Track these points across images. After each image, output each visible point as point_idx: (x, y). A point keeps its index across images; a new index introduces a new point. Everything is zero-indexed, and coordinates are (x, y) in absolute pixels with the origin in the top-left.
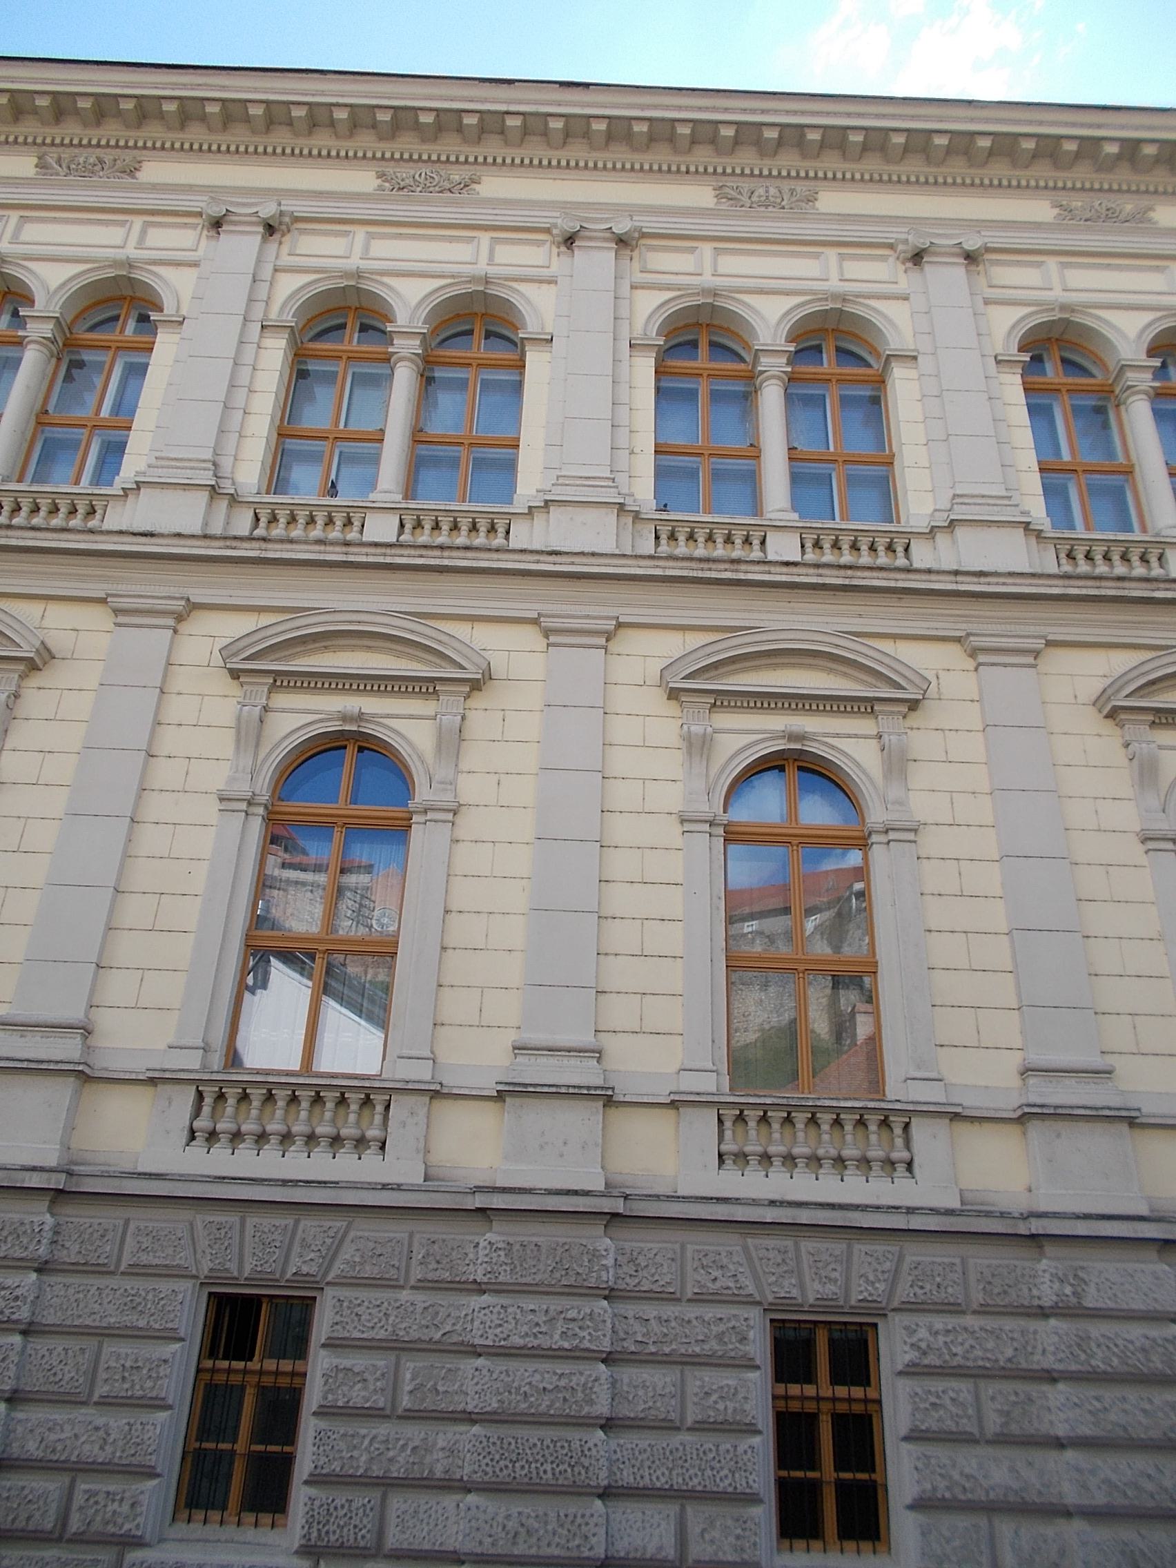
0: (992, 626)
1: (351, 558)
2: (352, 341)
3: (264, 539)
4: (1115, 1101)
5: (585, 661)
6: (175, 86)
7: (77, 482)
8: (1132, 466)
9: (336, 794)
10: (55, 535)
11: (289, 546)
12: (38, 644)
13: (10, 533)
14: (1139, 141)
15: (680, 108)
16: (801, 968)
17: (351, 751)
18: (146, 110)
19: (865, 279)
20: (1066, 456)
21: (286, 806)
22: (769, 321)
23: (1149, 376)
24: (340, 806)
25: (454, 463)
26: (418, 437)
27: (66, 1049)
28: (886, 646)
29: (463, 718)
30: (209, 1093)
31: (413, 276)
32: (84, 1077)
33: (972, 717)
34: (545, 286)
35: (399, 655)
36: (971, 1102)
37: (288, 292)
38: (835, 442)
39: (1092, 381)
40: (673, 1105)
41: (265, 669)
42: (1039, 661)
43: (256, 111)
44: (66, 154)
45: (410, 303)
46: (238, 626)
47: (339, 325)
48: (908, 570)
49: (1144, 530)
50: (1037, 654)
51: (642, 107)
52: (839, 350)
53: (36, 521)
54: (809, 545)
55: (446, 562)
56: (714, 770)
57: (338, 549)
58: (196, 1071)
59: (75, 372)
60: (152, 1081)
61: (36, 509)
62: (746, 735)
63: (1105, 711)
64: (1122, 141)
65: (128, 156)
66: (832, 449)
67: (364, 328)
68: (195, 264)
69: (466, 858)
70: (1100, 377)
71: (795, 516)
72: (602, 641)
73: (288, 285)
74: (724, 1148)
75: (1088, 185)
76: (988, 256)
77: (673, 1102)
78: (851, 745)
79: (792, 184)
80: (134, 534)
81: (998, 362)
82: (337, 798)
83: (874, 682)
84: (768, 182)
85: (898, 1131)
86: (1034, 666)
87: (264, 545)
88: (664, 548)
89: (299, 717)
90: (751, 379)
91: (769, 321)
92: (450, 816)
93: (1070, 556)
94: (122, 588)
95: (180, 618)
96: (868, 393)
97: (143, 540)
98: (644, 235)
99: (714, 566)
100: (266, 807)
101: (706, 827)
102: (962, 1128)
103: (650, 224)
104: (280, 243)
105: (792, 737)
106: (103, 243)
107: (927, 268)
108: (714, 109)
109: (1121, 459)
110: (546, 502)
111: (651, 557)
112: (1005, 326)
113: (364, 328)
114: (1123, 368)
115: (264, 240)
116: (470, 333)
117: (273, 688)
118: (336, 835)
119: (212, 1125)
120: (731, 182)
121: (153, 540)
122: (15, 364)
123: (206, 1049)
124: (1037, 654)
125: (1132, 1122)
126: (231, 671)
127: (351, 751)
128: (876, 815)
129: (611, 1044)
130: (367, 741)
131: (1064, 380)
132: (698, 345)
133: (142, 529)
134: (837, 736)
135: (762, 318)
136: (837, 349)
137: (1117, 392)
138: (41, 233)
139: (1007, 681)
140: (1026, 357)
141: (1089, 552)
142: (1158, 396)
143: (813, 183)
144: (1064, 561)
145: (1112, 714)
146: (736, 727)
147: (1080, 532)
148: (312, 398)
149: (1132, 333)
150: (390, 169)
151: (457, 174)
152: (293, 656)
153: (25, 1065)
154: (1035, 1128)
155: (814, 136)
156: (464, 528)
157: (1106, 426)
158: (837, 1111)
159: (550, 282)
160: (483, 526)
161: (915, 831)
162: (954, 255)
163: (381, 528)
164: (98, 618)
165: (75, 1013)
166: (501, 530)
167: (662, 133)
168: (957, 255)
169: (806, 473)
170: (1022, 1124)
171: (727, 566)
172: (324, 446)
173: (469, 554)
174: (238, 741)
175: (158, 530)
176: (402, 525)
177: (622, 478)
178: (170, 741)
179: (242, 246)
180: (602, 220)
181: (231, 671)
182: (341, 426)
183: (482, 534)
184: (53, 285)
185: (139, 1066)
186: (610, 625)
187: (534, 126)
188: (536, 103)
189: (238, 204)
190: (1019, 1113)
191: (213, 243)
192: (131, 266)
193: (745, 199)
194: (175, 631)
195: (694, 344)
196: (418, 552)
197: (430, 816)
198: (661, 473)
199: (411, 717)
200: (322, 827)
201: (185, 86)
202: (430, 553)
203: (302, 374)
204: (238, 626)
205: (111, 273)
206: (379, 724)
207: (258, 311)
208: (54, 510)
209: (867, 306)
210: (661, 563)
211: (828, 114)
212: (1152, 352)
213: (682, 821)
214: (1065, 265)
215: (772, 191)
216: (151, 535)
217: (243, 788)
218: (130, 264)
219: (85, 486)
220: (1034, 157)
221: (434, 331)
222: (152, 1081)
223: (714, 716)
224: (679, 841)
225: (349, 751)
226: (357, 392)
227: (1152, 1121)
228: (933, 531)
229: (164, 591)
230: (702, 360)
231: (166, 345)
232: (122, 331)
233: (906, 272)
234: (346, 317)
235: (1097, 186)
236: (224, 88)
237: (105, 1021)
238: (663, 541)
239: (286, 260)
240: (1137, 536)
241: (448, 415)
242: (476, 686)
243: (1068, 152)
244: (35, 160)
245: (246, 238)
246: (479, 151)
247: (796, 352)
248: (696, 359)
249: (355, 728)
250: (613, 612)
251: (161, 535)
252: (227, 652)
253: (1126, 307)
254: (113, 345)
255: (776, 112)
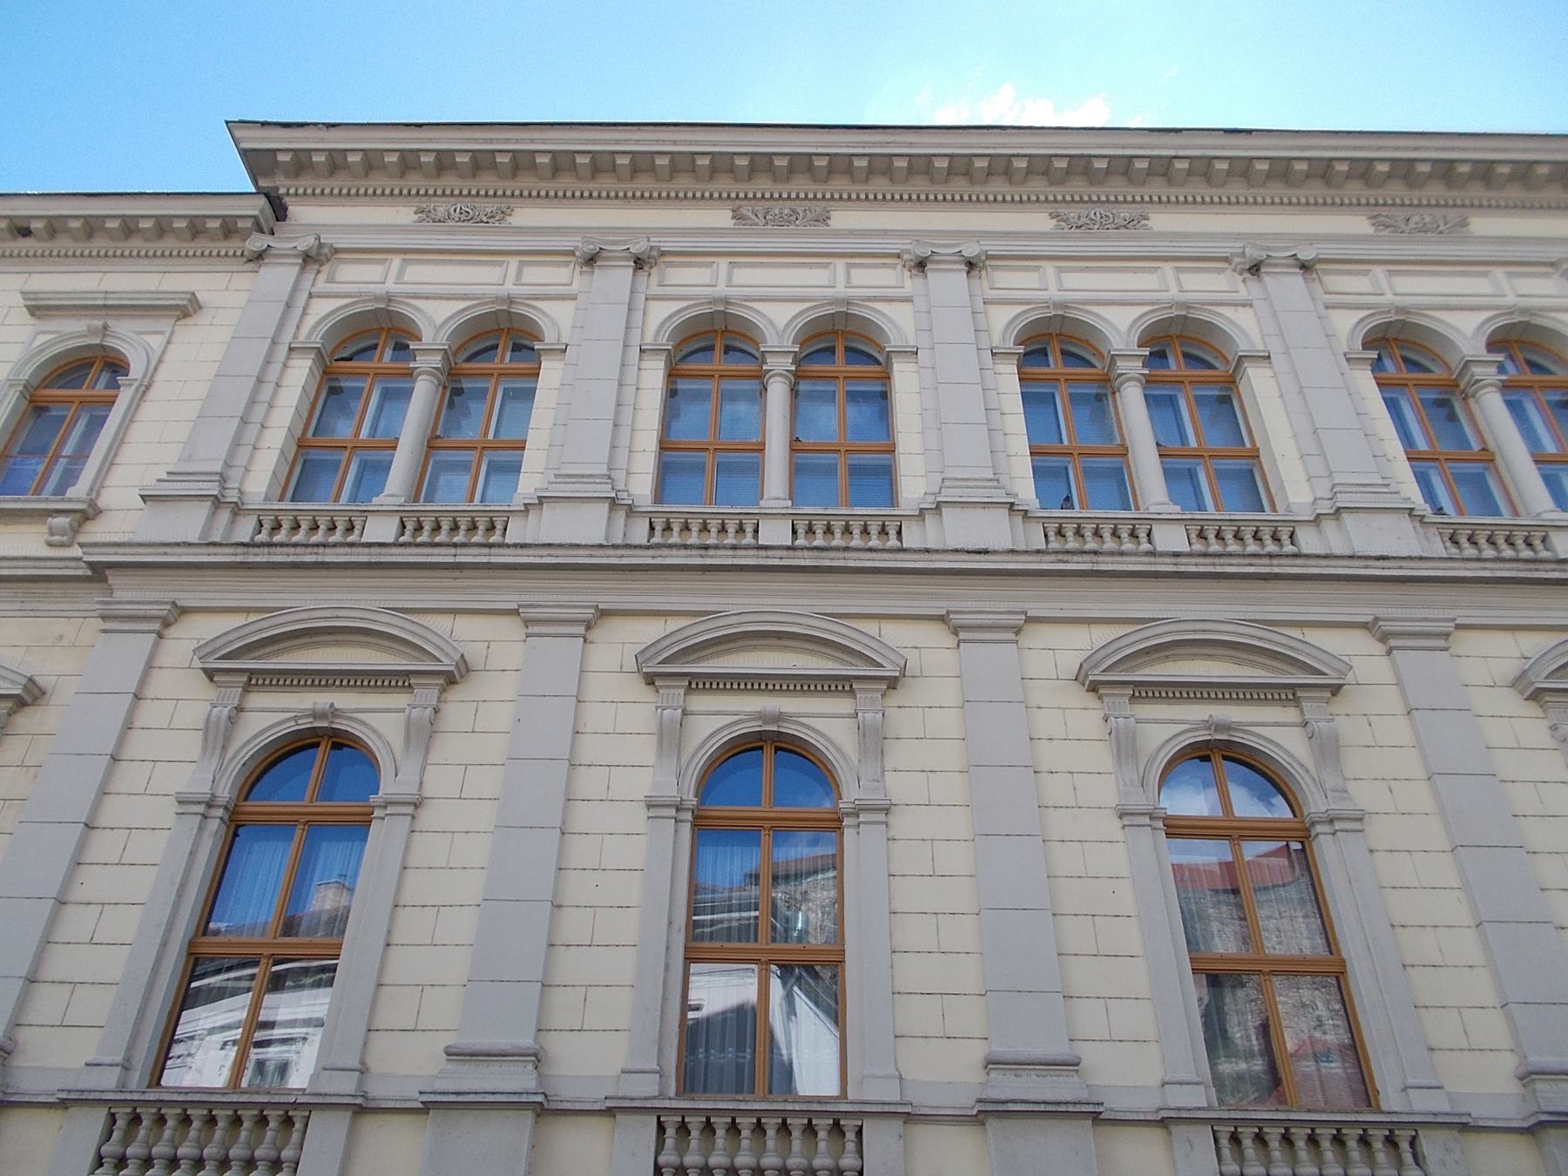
0: (973, 602)
1: (1182, 569)
2: (505, 359)
3: (1095, 553)
4: (1084, 1095)
5: (561, 651)
6: (865, 144)
7: (337, 500)
8: (1258, 450)
9: (301, 792)
10: (891, 556)
11: (1119, 559)
12: (457, 657)
13: (847, 555)
14: (1452, 162)
15: (1336, 148)
16: (764, 958)
17: (768, 752)
18: (522, 163)
19: (871, 287)
20: (1193, 443)
21: (716, 810)
22: (1120, 329)
23: (1493, 370)
24: (764, 809)
25: (700, 468)
26: (795, 446)
27: (516, 1080)
28: (870, 627)
29: (436, 711)
30: (123, 1113)
31: (439, 296)
32: (545, 1110)
33: (948, 693)
34: (1241, 309)
35: (1240, 662)
36: (926, 1100)
37: (660, 318)
38: (1069, 436)
39: (1093, 371)
40: (1164, 1123)
41: (675, 673)
42: (1019, 638)
43: (426, 159)
44: (760, 207)
45: (436, 322)
46: (651, 631)
47: (710, 347)
48: (1296, 556)
49: (1516, 514)
50: (1018, 631)
51: (1302, 149)
52: (1064, 353)
53: (277, 538)
54: (1051, 534)
55: (1276, 570)
56: (685, 758)
57: (1167, 560)
58: (654, 1098)
59: (456, 399)
60: (610, 1112)
61: (296, 527)
62: (1167, 727)
63: (1527, 694)
64: (1435, 161)
65: (818, 207)
66: (1066, 442)
67: (517, 348)
68: (573, 298)
69: (424, 851)
70: (1439, 373)
71: (1178, 509)
72: (581, 630)
73: (321, 308)
74: (662, 1159)
75: (1398, 201)
76: (1318, 266)
77: (1163, 1119)
78: (1275, 731)
79: (1444, 211)
80: (969, 552)
81: (1348, 360)
82: (763, 803)
83: (1285, 667)
84: (1422, 211)
85: (850, 1135)
86: (1446, 649)
87: (1095, 558)
88: (1055, 544)
89: (718, 718)
90: (760, 377)
91: (1120, 329)
92: (410, 810)
93: (1201, 535)
94: (954, 605)
95: (167, 624)
96: (879, 389)
97: (977, 557)
98: (989, 257)
99: (1541, 566)
100: (226, 808)
101: (1147, 820)
102: (1472, 1138)
103: (668, 244)
104: (319, 272)
105: (1219, 727)
106: (487, 281)
107: (1266, 278)
108: (1370, 148)
109: (1476, 447)
110: (939, 503)
111: (788, 548)
112: (1347, 326)
113: (728, 349)
114: (1467, 364)
115: (303, 268)
116: (711, 348)
117: (247, 688)
118: (298, 832)
119: (222, 1152)
120: (1385, 211)
121: (986, 557)
122: (407, 394)
123: (126, 1067)
124: (1447, 635)
125: (1096, 1118)
126: (205, 670)
127: (768, 752)
128: (1315, 804)
129: (1087, 1053)
130: (1230, 750)
131: (1410, 375)
132: (1054, 353)
133: (976, 547)
134: (1262, 725)
135: (1458, 331)
136: (844, 351)
137: (1462, 386)
138: (423, 274)
139: (990, 657)
140: (1146, 352)
141: (1133, 530)
142: (1149, 382)
143: (1462, 210)
144: (1449, 544)
145: (1094, 688)
146: (1159, 717)
147: (1211, 512)
148: (466, 413)
149: (1124, 326)
150: (1063, 210)
151: (1125, 213)
152: (1139, 666)
153: (1042, 1107)
154: (992, 1124)
155: (901, 163)
156: (695, 528)
157: (1452, 417)
158: (1287, 1126)
159: (1244, 305)
160: (874, 529)
161: (887, 811)
162: (955, 262)
163: (381, 530)
164: (509, 629)
165: (526, 1041)
166: (749, 529)
167: (1323, 171)
168: (627, 259)
169: (1179, 468)
170: (983, 1124)
171: (1553, 566)
172: (472, 456)
173: (1298, 561)
174: (206, 739)
175: (991, 548)
176: (652, 528)
177: (620, 476)
178: (590, 749)
179: (618, 278)
180: (1288, 248)
181: (205, 670)
182: (491, 436)
183: (695, 534)
184: (781, 322)
185: (595, 1095)
186: (164, 610)
187: (1202, 169)
188: (1202, 147)
189: (939, 246)
190: (1533, 1121)
191: (586, 278)
192: (728, 303)
193: (1402, 225)
194: (160, 636)
195: (831, 350)
196: (1247, 561)
197: (1338, 825)
198: (1037, 472)
199: (1276, 724)
200: (279, 826)
201: (875, 144)
202: (1258, 561)
203: (334, 391)
204: (651, 631)
205: (706, 310)
206: (350, 719)
207: (635, 340)
208: (315, 528)
209: (1431, 318)
210: (1488, 565)
211: (1475, 150)
212: (1367, 345)
213: (649, 806)
214: (1060, 270)
215: (1427, 219)
216: (986, 552)
217: (670, 792)
218: (510, 300)
219: (343, 503)
220: (830, 172)
221: (677, 347)
222: (610, 1112)
223: (689, 698)
224: (1119, 835)
225: (326, 747)
226: (509, 406)
227: (578, 1106)
228: (1318, 519)
229: (1003, 606)
230: (840, 364)
231: (551, 373)
232: (380, 359)
233: (1244, 281)
234: (499, 338)
235: (1416, 202)
236: (911, 145)
237: (556, 1045)
238: (658, 532)
239: (655, 289)
240: (1507, 519)
241: (694, 423)
242: (450, 680)
243: (1502, 175)
244: (730, 214)
245: (622, 270)
246: (1145, 192)
247: (1025, 354)
248: (711, 361)
249: (325, 725)
250: (170, 596)
251: (995, 552)
252: (202, 651)
253: (1462, 309)
254: (841, 375)
255: (1427, 149)
